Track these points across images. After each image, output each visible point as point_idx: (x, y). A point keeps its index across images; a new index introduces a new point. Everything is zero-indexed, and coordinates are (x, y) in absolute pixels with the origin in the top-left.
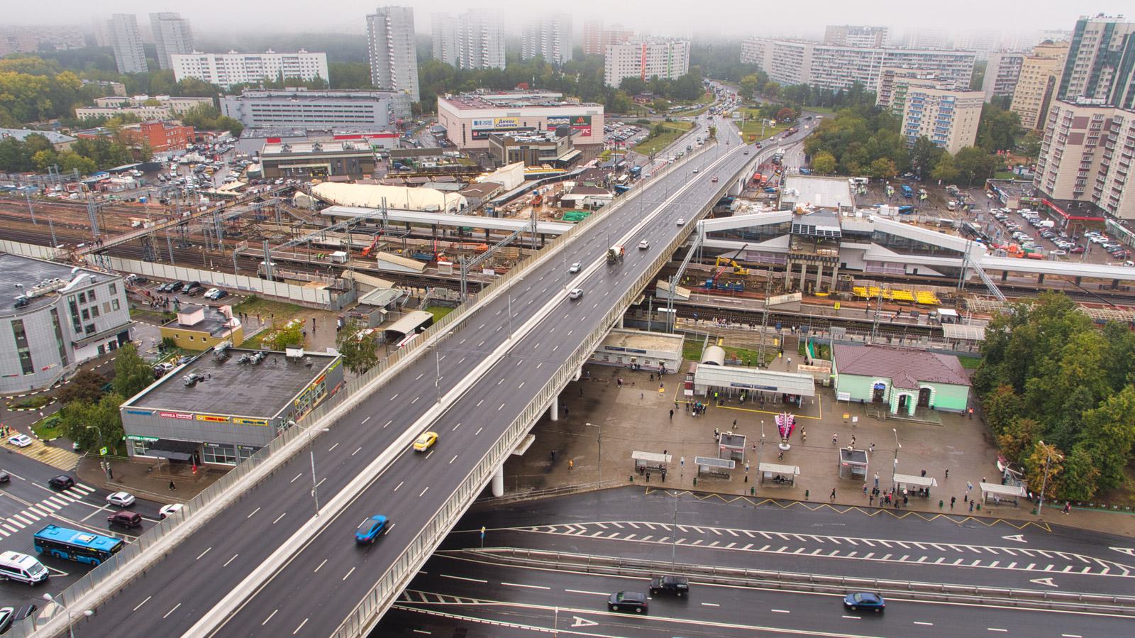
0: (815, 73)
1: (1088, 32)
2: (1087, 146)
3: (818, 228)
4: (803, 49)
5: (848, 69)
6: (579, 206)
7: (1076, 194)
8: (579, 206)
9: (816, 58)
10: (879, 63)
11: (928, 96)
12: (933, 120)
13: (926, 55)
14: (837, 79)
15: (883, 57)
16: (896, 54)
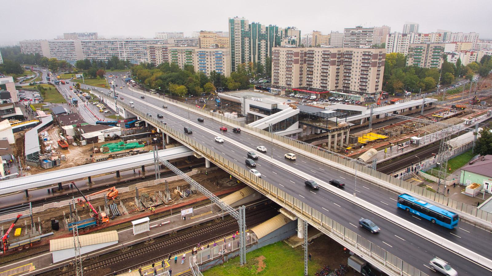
0: (86, 54)
1: (236, 24)
2: (300, 64)
3: (398, 103)
4: (73, 42)
5: (105, 50)
6: (102, 140)
7: (300, 85)
8: (102, 140)
9: (84, 46)
10: (125, 46)
11: (207, 52)
12: (213, 63)
13: (143, 41)
14: (101, 56)
15: (123, 43)
16: (129, 42)
